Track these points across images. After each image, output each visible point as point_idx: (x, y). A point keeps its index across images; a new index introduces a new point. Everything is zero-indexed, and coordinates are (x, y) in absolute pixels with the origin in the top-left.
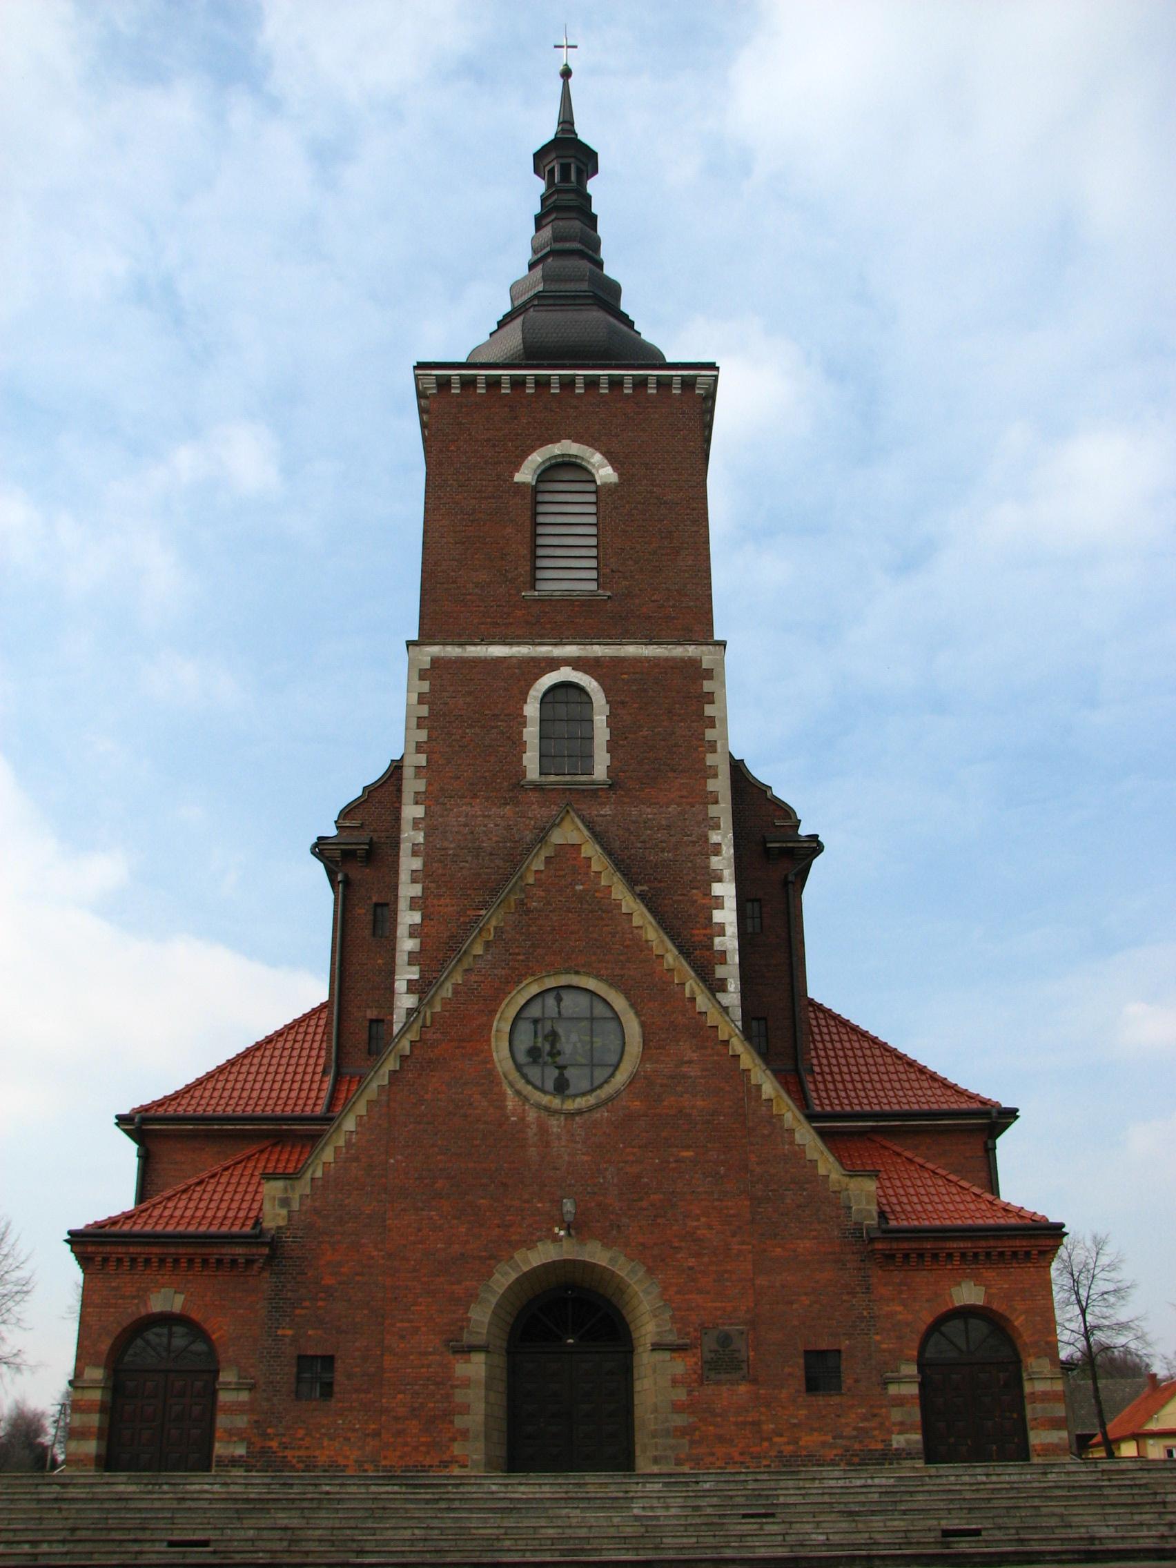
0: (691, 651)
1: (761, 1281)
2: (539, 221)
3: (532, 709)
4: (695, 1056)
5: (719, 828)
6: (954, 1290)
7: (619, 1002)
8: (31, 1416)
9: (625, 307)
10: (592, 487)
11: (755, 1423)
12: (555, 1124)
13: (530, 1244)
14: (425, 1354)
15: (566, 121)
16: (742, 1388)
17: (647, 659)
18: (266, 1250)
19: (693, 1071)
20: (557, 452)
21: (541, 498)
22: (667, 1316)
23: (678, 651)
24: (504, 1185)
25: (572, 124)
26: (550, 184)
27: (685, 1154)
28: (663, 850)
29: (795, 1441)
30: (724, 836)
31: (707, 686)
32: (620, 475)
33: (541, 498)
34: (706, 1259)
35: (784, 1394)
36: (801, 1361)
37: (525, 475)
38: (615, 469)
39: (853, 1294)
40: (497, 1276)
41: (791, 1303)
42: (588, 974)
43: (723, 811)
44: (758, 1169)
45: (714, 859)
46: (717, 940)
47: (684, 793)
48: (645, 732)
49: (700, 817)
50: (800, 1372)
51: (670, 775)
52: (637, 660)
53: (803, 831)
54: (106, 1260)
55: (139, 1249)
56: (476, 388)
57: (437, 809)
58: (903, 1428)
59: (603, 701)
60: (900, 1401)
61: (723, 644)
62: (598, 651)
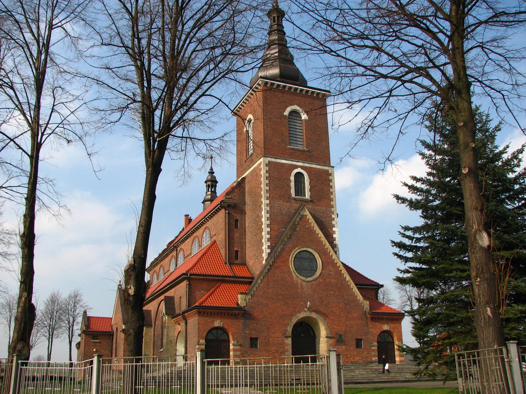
0: (327, 168)
1: (347, 323)
3: (292, 178)
4: (332, 269)
6: (384, 326)
7: (317, 255)
8: (18, 334)
11: (347, 355)
12: (304, 284)
13: (300, 313)
14: (279, 337)
16: (344, 347)
17: (317, 169)
18: (243, 312)
19: (333, 273)
20: (294, 108)
22: (328, 330)
23: (324, 168)
24: (294, 298)
27: (331, 293)
29: (354, 359)
34: (336, 317)
35: (352, 348)
36: (355, 341)
37: (286, 113)
38: (307, 116)
39: (365, 326)
40: (293, 319)
41: (353, 328)
42: (310, 248)
44: (346, 297)
45: (333, 222)
46: (334, 242)
50: (355, 344)
52: (315, 169)
54: (204, 313)
55: (213, 311)
57: (272, 201)
58: (374, 356)
60: (374, 350)
61: (333, 167)
62: (306, 165)
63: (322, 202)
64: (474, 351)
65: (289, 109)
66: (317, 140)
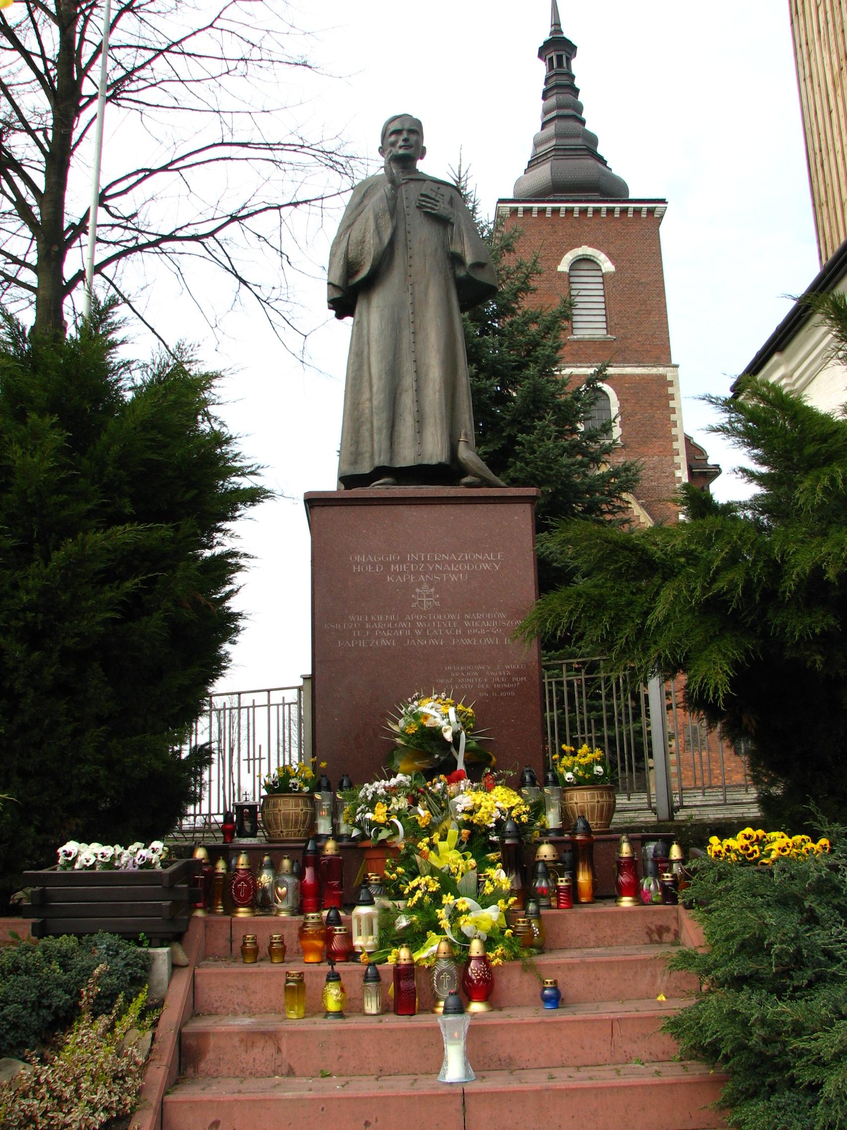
0: (661, 370)
2: (545, 96)
5: (680, 468)
9: (600, 150)
10: (599, 274)
15: (556, 25)
17: (638, 375)
21: (572, 280)
25: (559, 25)
26: (551, 67)
28: (652, 481)
30: (683, 473)
31: (670, 390)
32: (616, 267)
33: (572, 280)
37: (563, 267)
38: (613, 263)
43: (681, 459)
47: (661, 449)
48: (639, 416)
49: (670, 463)
51: (654, 440)
52: (632, 376)
53: (711, 462)
56: (531, 214)
59: (616, 399)
61: (676, 366)
63: (651, 446)
64: (560, 662)
65: (569, 257)
66: (637, 313)
